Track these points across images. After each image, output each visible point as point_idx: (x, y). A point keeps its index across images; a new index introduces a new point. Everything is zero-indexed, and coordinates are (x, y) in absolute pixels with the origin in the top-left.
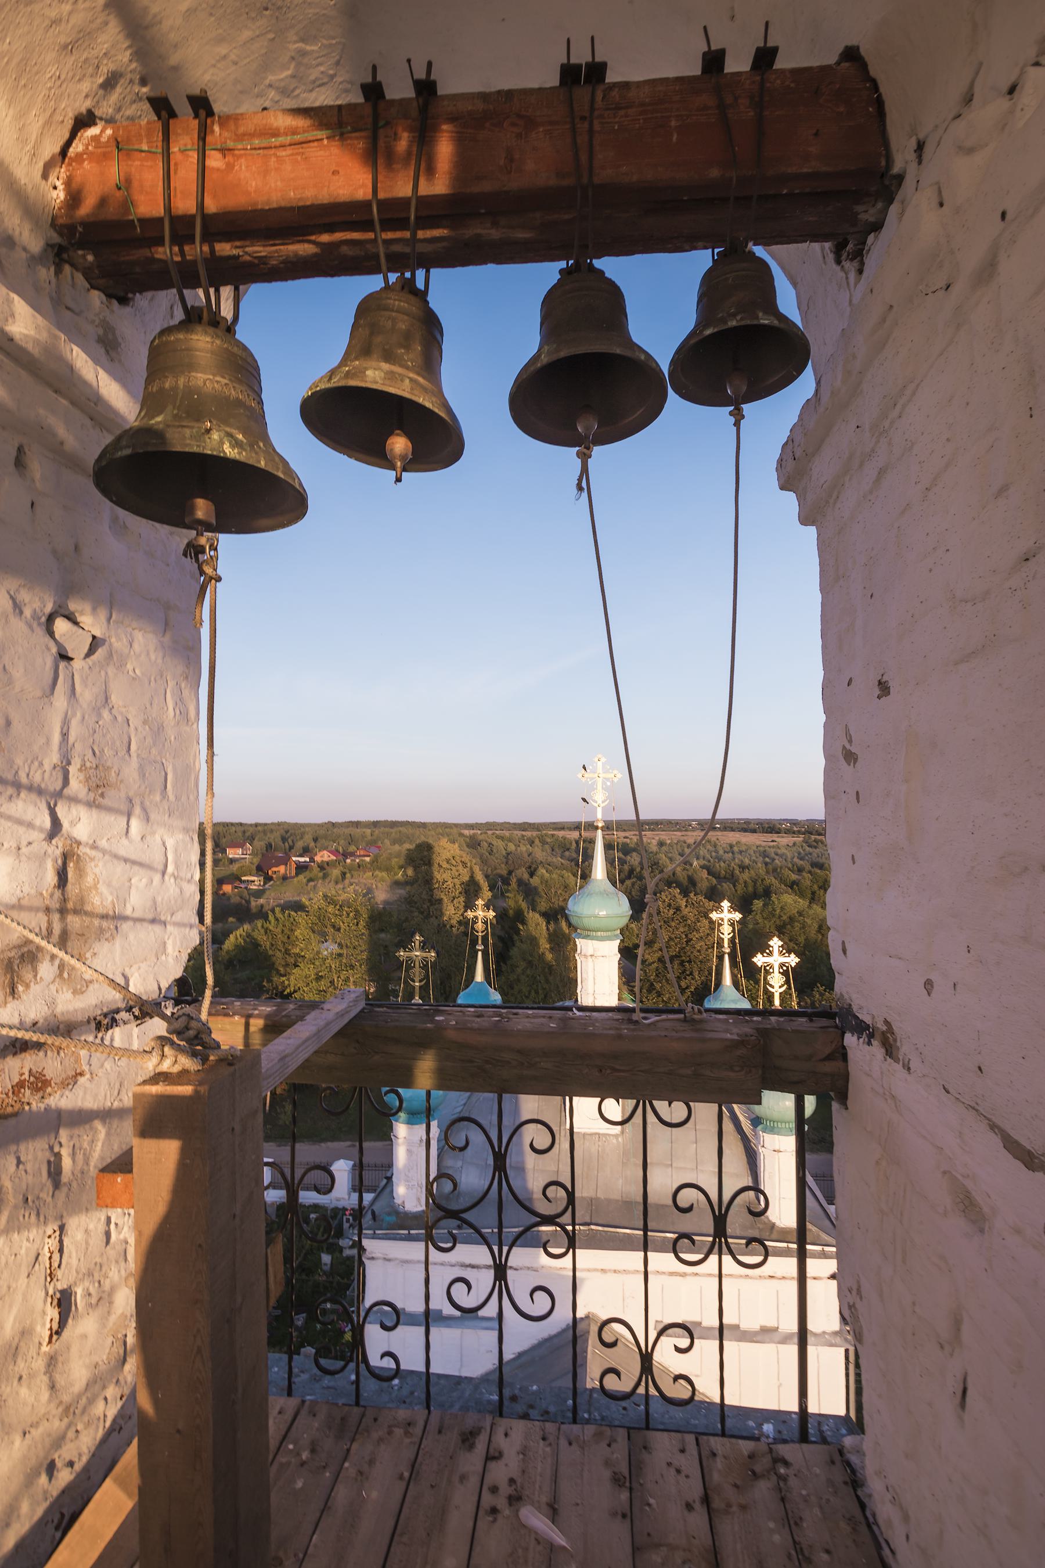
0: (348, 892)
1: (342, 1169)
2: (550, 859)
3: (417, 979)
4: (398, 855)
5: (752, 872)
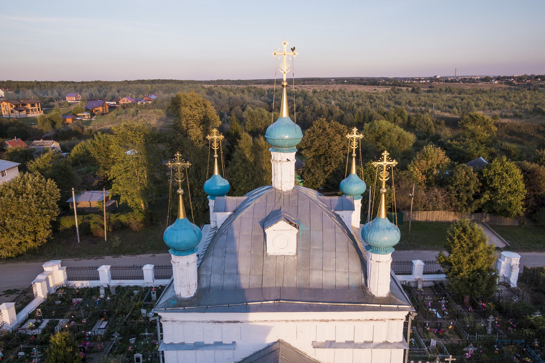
0: (138, 123)
1: (148, 270)
2: (253, 101)
3: (179, 178)
4: (168, 100)
5: (363, 107)
